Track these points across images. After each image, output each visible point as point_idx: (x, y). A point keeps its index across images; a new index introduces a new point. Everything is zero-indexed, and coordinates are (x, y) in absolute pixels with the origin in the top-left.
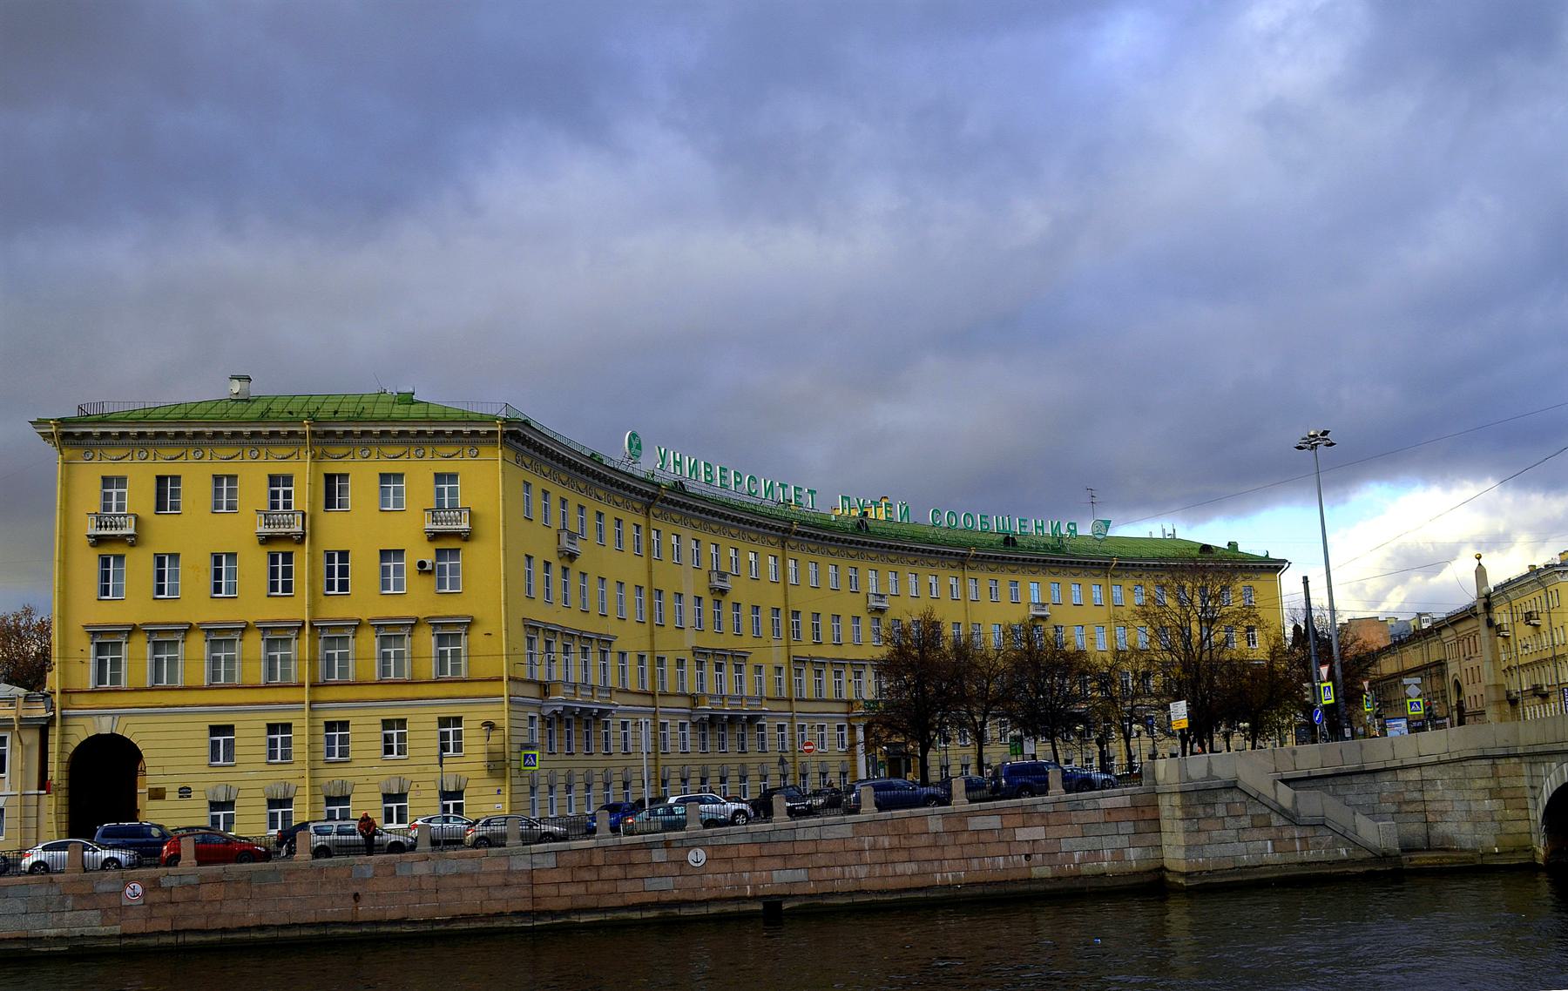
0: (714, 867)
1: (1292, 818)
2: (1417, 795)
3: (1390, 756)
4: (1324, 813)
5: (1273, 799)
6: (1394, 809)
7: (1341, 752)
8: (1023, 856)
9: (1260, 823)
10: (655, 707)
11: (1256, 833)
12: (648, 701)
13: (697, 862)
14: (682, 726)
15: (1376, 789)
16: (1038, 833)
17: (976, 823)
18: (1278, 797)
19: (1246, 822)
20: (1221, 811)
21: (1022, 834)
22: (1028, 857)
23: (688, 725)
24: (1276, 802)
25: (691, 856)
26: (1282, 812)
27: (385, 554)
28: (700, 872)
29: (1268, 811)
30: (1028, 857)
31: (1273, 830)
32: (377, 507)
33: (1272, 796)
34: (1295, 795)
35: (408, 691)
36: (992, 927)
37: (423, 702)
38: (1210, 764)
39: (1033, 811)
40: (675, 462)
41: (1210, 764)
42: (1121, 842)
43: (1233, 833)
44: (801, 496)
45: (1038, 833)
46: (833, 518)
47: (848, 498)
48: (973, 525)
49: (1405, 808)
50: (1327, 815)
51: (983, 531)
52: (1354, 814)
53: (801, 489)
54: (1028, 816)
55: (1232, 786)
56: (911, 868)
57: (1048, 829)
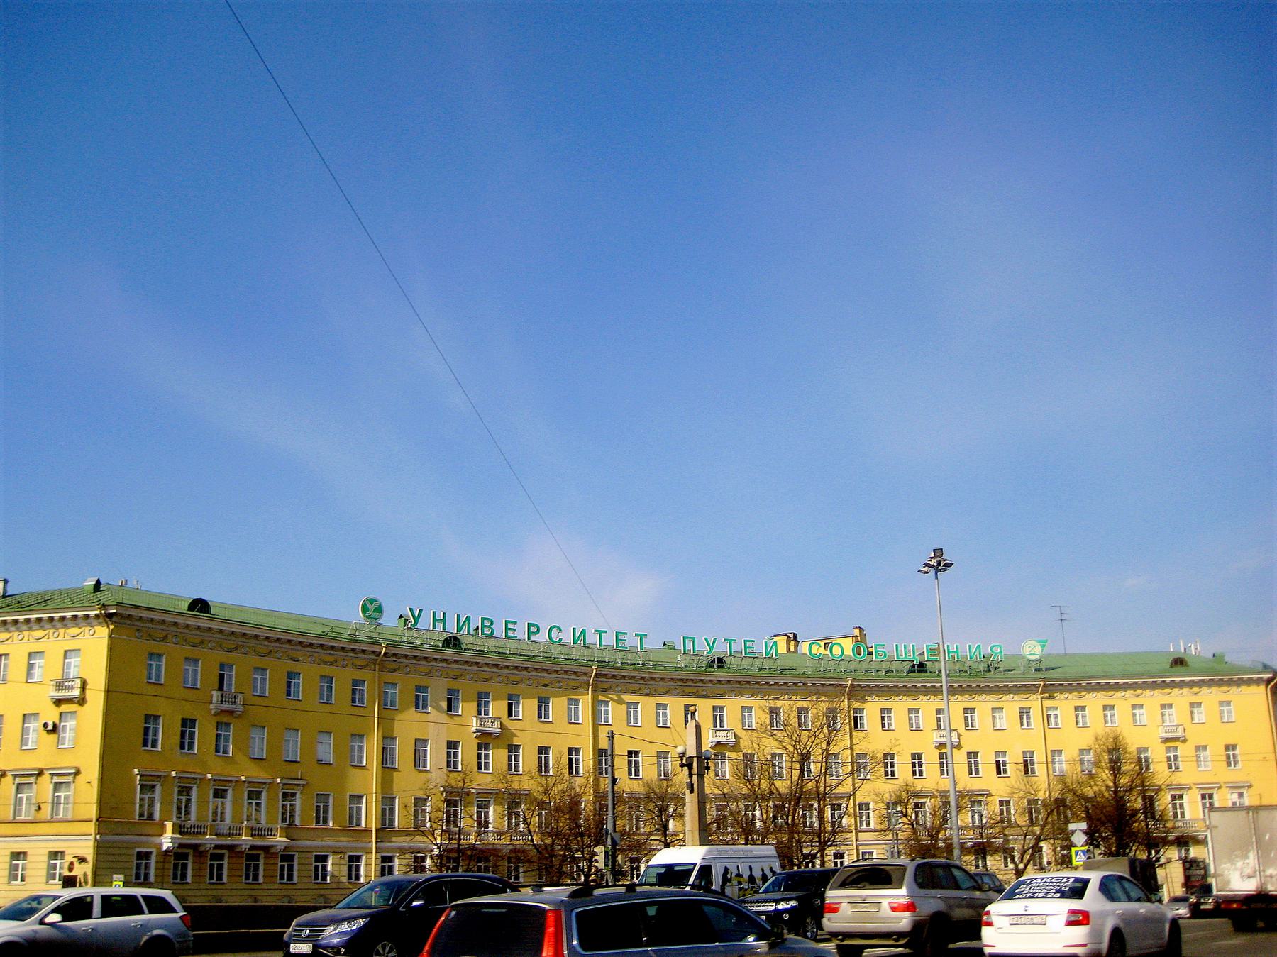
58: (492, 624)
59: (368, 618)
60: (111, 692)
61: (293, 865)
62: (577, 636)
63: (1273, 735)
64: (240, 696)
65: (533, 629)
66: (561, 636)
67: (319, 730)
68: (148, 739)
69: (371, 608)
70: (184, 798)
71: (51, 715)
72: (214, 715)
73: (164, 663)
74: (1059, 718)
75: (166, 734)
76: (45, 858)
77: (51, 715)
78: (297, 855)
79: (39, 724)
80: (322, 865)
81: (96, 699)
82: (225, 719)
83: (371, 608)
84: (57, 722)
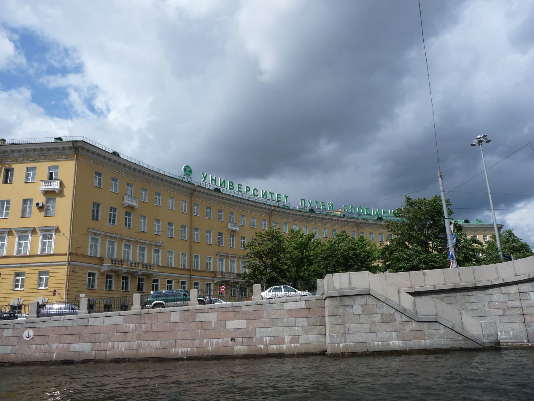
0: (37, 340)
1: (413, 318)
2: (518, 304)
3: (496, 277)
4: (437, 313)
5: (398, 303)
6: (500, 312)
7: (459, 274)
8: (230, 339)
9: (388, 319)
10: (190, 275)
11: (385, 327)
12: (187, 273)
13: (28, 337)
14: (209, 285)
15: (487, 299)
16: (240, 324)
17: (201, 317)
18: (401, 302)
19: (377, 318)
20: (357, 310)
21: (231, 325)
22: (232, 339)
23: (212, 284)
24: (400, 305)
25: (25, 334)
26: (403, 312)
27: (25, 201)
28: (28, 343)
29: (393, 311)
30: (232, 339)
31: (397, 324)
32: (24, 181)
33: (397, 301)
34: (415, 301)
35: (27, 260)
36: (491, 371)
37: (38, 264)
38: (350, 278)
39: (239, 310)
40: (212, 180)
41: (350, 278)
42: (298, 330)
43: (366, 326)
44: (280, 198)
45: (240, 324)
46: (298, 207)
47: (304, 200)
48: (362, 211)
49: (508, 312)
50: (439, 314)
51: (368, 215)
52: (461, 314)
53: (280, 195)
54: (236, 314)
55: (367, 294)
56: (157, 344)
57: (248, 321)
58: (233, 184)
59: (187, 174)
60: (77, 188)
61: (4, 243)
62: (263, 194)
63: (75, 178)
64: (136, 200)
65: (248, 189)
66: (258, 193)
67: (12, 184)
68: (95, 217)
69: (188, 170)
70: (143, 258)
71: (42, 200)
72: (124, 207)
73: (383, 236)
74: (374, 237)
75: (104, 214)
76: (13, 276)
77: (42, 200)
78: (160, 280)
79: (34, 203)
80: (170, 285)
81: (69, 192)
82: (233, 234)
83: (188, 170)
84: (44, 203)
